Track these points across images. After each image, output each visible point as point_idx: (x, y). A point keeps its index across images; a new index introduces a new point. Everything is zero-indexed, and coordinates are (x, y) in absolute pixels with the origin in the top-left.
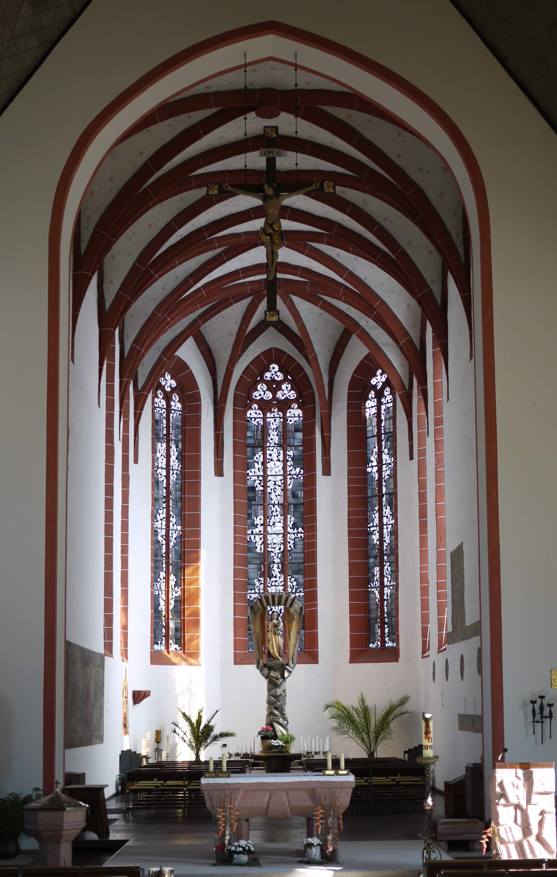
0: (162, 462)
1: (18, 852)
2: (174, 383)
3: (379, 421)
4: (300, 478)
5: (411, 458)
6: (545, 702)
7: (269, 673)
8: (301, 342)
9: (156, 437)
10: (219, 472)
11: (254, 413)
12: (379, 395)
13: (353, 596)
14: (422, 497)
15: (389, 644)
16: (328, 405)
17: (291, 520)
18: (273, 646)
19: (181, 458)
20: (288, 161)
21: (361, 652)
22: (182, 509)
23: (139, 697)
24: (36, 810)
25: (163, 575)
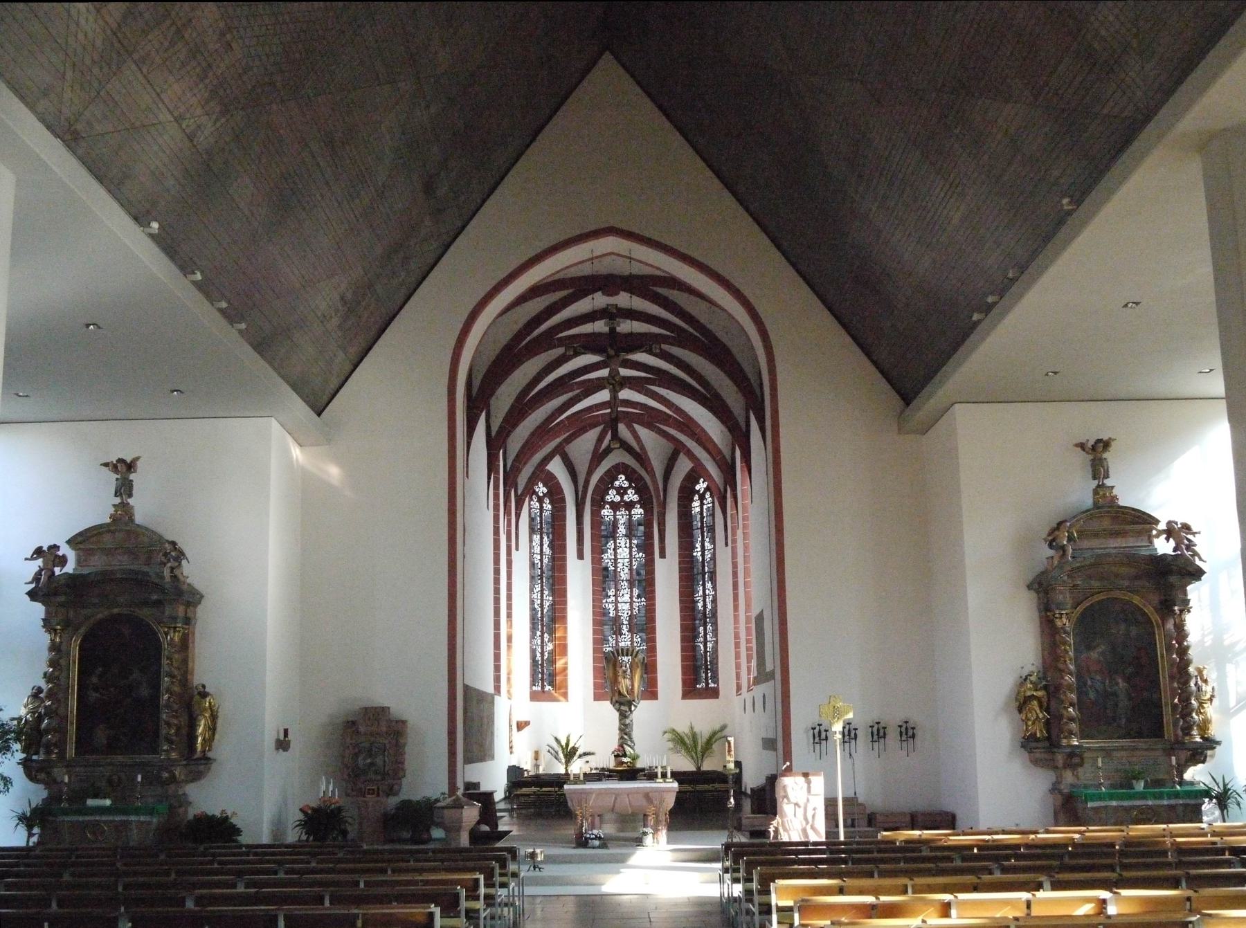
0: (537, 549)
1: (430, 839)
2: (545, 490)
3: (702, 518)
5: (727, 544)
6: (822, 728)
8: (641, 457)
9: (532, 531)
10: (580, 556)
11: (607, 512)
12: (702, 498)
13: (683, 649)
14: (735, 574)
15: (712, 685)
16: (663, 505)
17: (636, 592)
19: (551, 546)
20: (626, 326)
21: (690, 692)
22: (553, 585)
23: (521, 726)
24: (443, 808)
25: (539, 633)
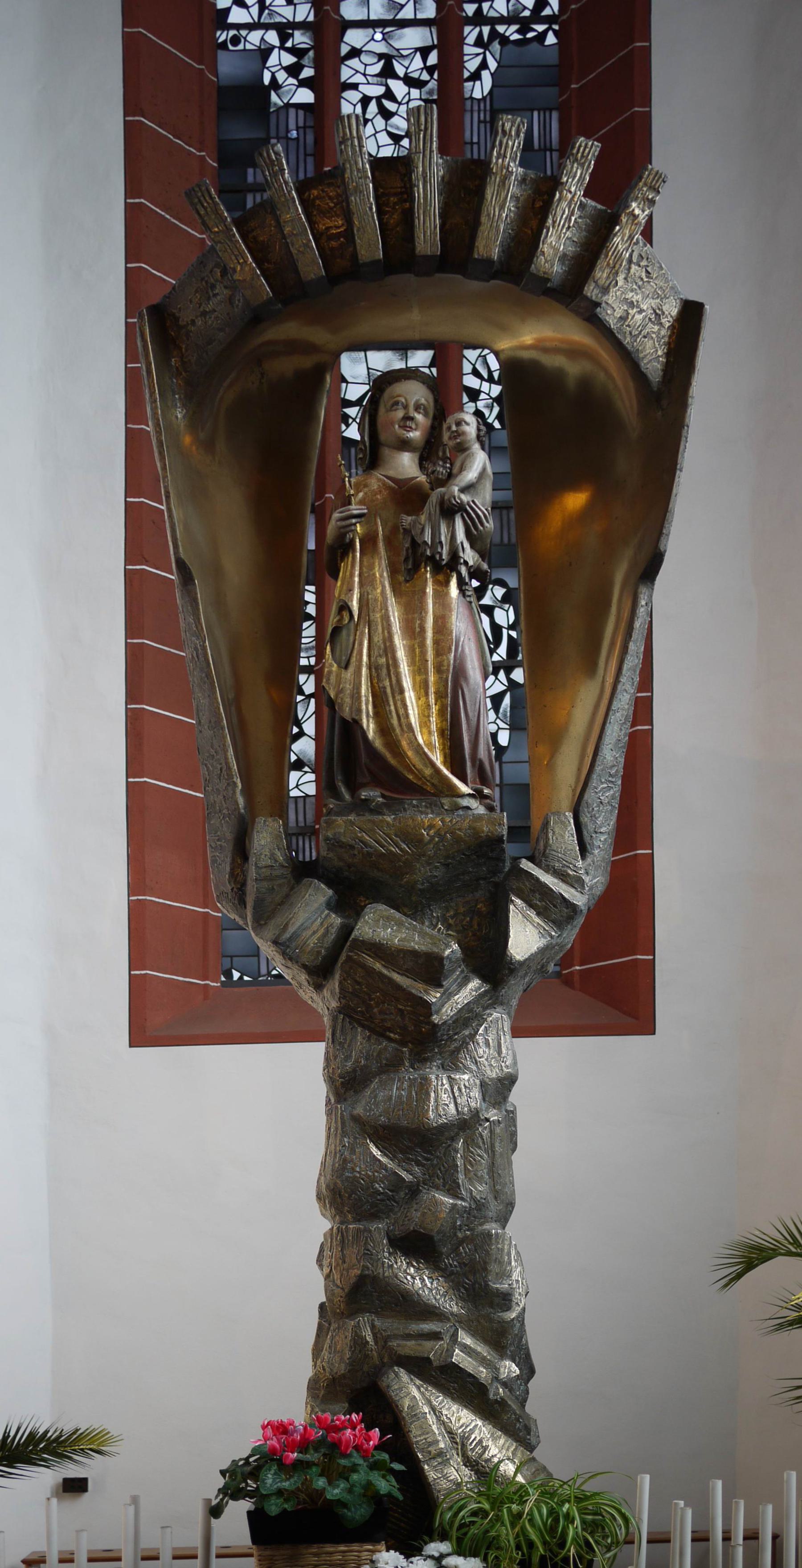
4: (542, 36)
7: (346, 932)
18: (384, 670)
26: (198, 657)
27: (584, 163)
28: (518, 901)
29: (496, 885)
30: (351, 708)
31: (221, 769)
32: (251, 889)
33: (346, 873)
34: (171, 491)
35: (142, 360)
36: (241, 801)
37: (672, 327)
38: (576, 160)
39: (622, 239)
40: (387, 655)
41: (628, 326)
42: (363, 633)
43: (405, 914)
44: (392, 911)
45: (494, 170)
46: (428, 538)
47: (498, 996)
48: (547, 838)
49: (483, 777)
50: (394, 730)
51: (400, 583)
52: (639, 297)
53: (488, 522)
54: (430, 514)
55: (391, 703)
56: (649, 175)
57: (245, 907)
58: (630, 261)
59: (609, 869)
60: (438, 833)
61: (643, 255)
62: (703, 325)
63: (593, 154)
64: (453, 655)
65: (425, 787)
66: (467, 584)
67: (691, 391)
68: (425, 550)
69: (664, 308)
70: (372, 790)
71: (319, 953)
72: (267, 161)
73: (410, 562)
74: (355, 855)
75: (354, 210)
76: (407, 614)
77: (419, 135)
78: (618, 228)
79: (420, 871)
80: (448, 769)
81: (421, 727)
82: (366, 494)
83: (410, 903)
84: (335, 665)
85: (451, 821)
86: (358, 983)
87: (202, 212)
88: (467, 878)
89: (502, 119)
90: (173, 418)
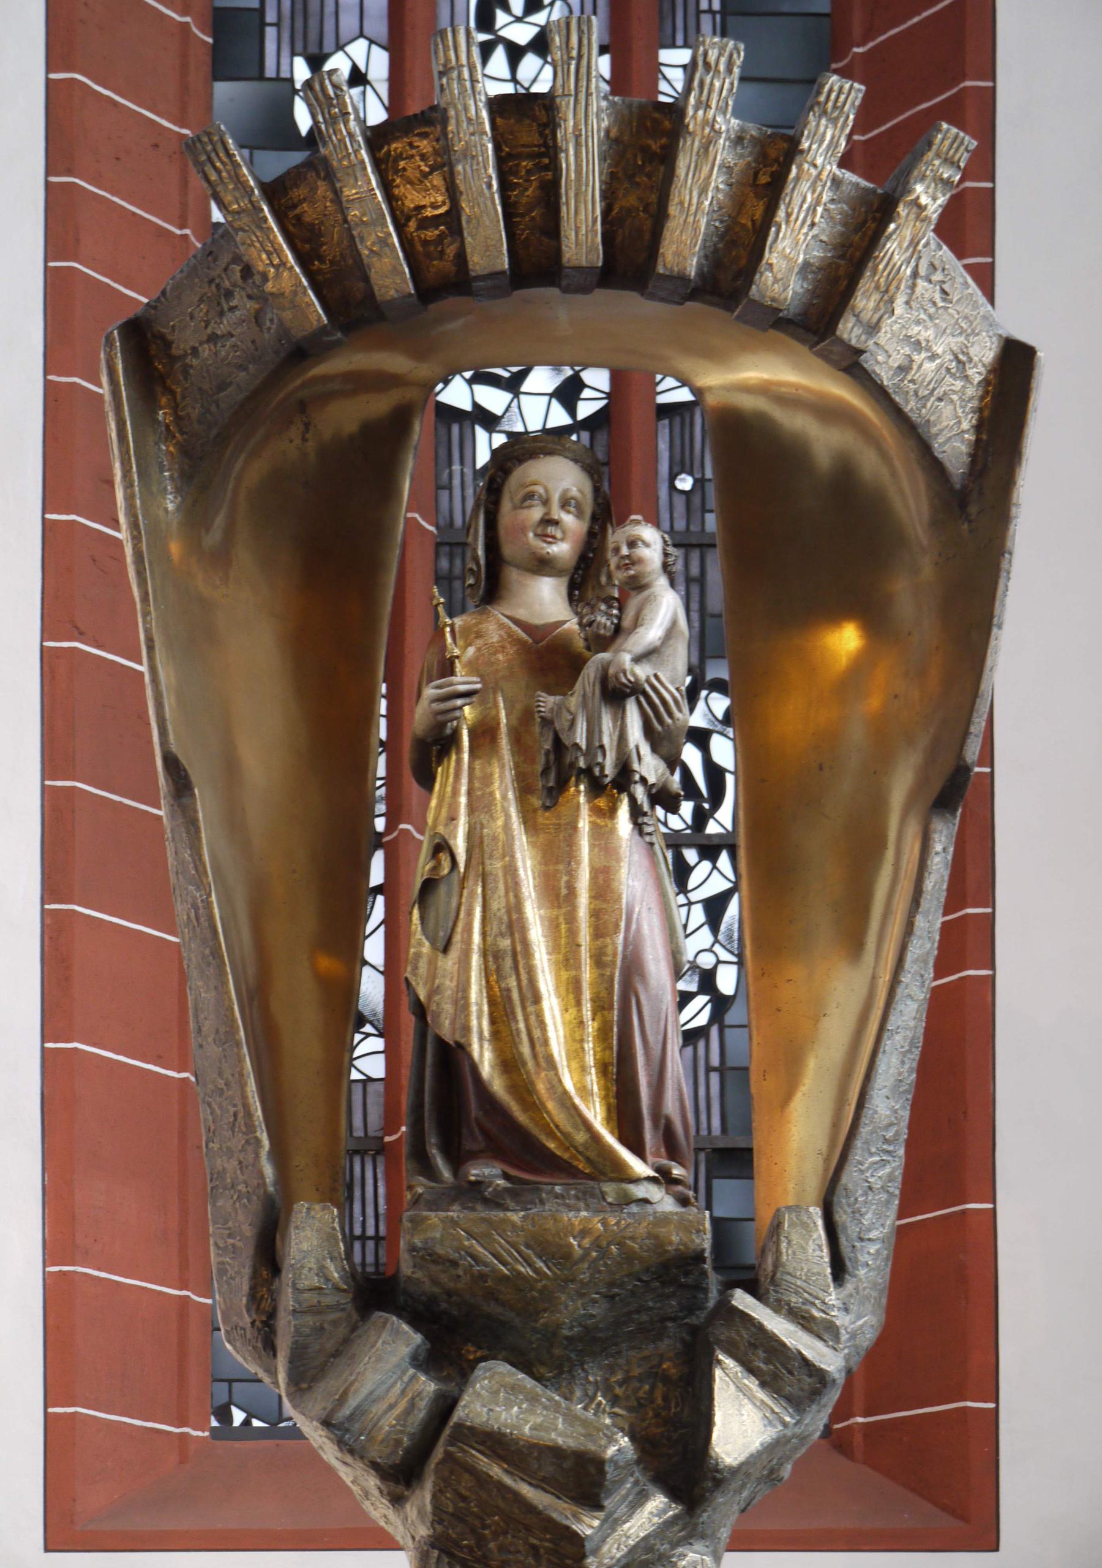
7: (445, 1406)
18: (507, 958)
26: (197, 919)
27: (837, 119)
28: (729, 1362)
29: (694, 1331)
30: (453, 1022)
31: (235, 1115)
32: (286, 1328)
33: (444, 1305)
34: (156, 637)
35: (104, 379)
36: (268, 1171)
37: (986, 382)
38: (824, 113)
39: (900, 245)
40: (512, 935)
41: (912, 381)
42: (472, 893)
43: (539, 1379)
44: (521, 1376)
45: (691, 127)
46: (580, 737)
47: (696, 1525)
48: (778, 1252)
49: (671, 1146)
50: (524, 1064)
51: (535, 811)
52: (930, 333)
53: (680, 710)
54: (584, 696)
55: (520, 1017)
56: (943, 139)
57: (275, 1355)
58: (915, 274)
59: (884, 1301)
60: (596, 1244)
61: (936, 263)
62: (1034, 384)
63: (853, 103)
64: (621, 936)
65: (575, 1163)
66: (645, 814)
67: (1015, 495)
68: (577, 758)
69: (972, 351)
70: (487, 1166)
71: (398, 1442)
72: (320, 95)
73: (552, 776)
74: (459, 1277)
75: (462, 188)
76: (546, 864)
77: (569, 65)
78: (892, 226)
79: (566, 1307)
80: (612, 1133)
81: (568, 1059)
82: (479, 649)
83: (547, 1360)
84: (427, 944)
85: (618, 1224)
86: (464, 1499)
87: (213, 177)
88: (644, 1317)
89: (704, 42)
90: (161, 513)
